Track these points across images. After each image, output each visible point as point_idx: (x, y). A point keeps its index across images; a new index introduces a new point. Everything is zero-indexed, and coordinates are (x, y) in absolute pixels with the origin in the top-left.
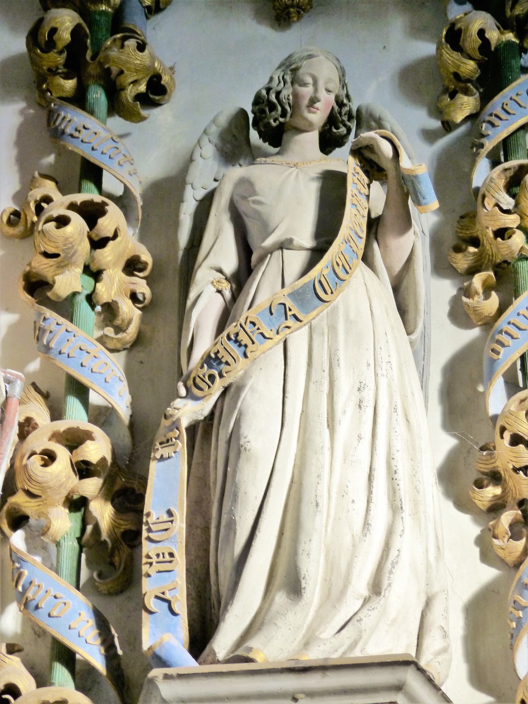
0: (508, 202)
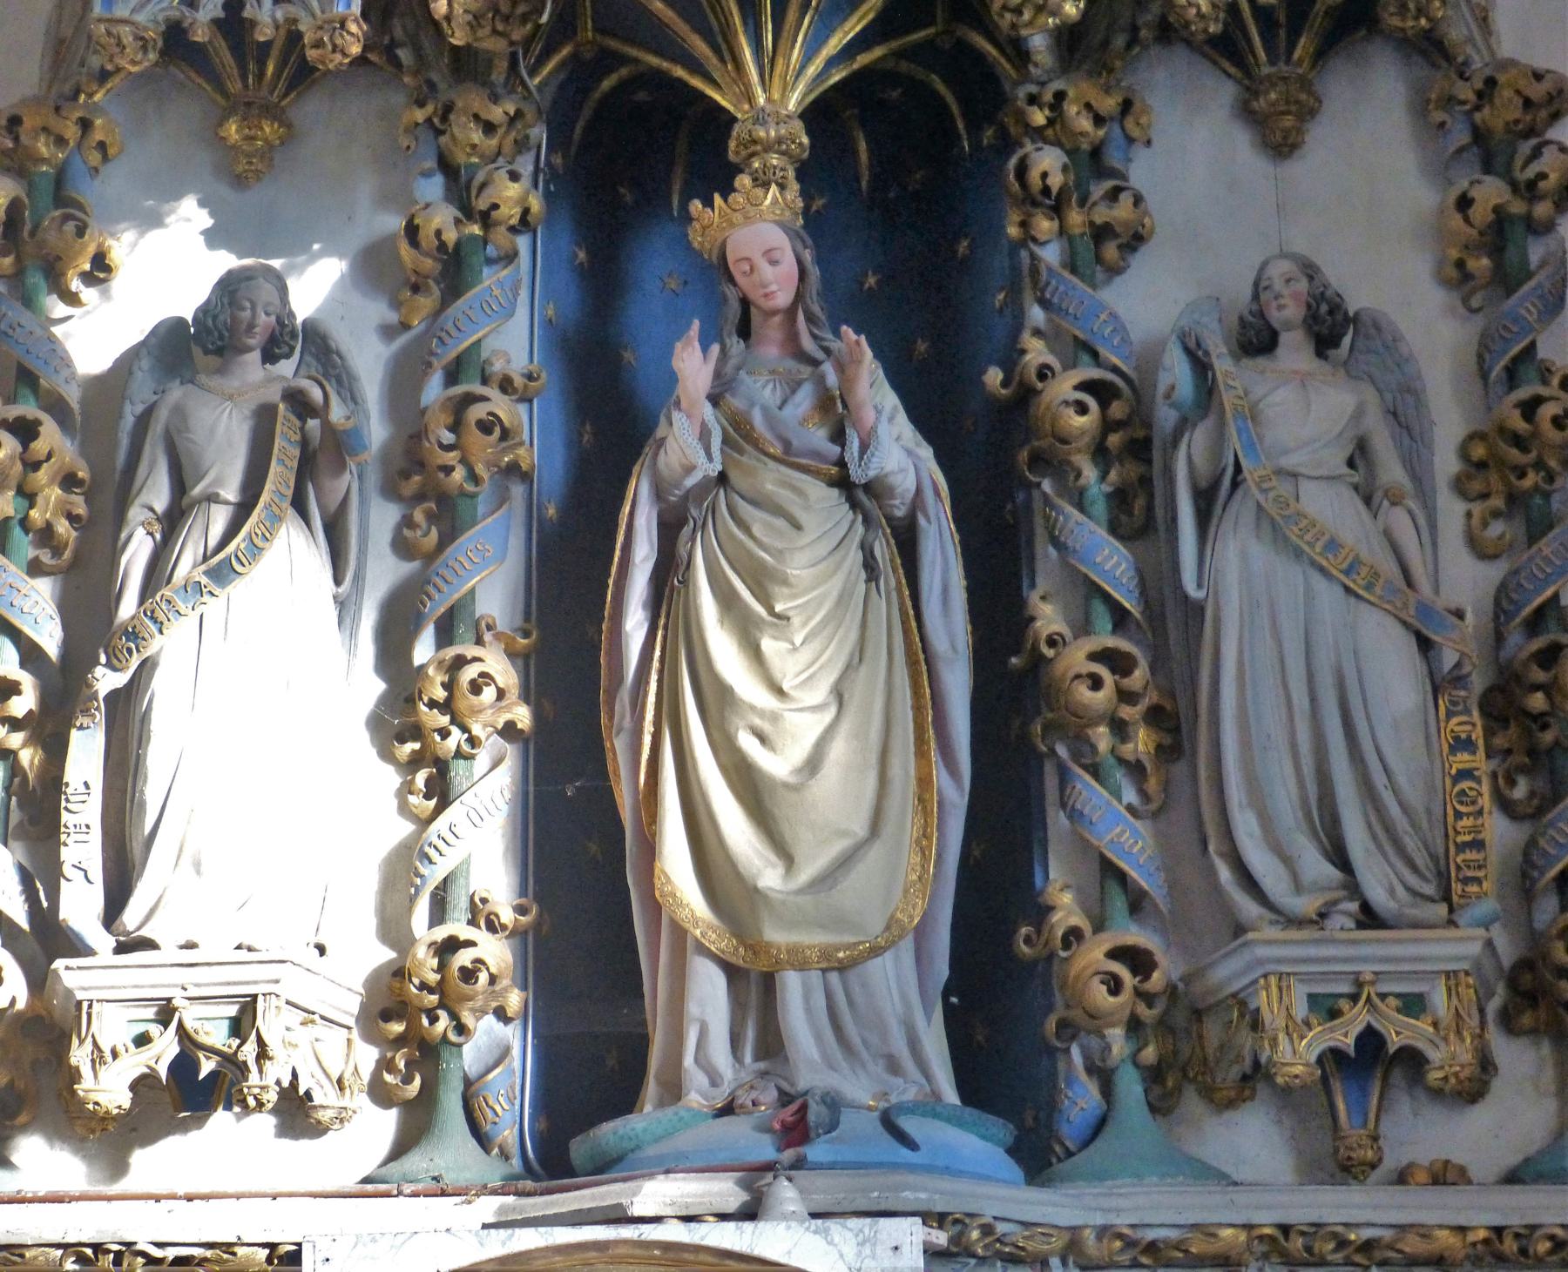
0: (448, 437)
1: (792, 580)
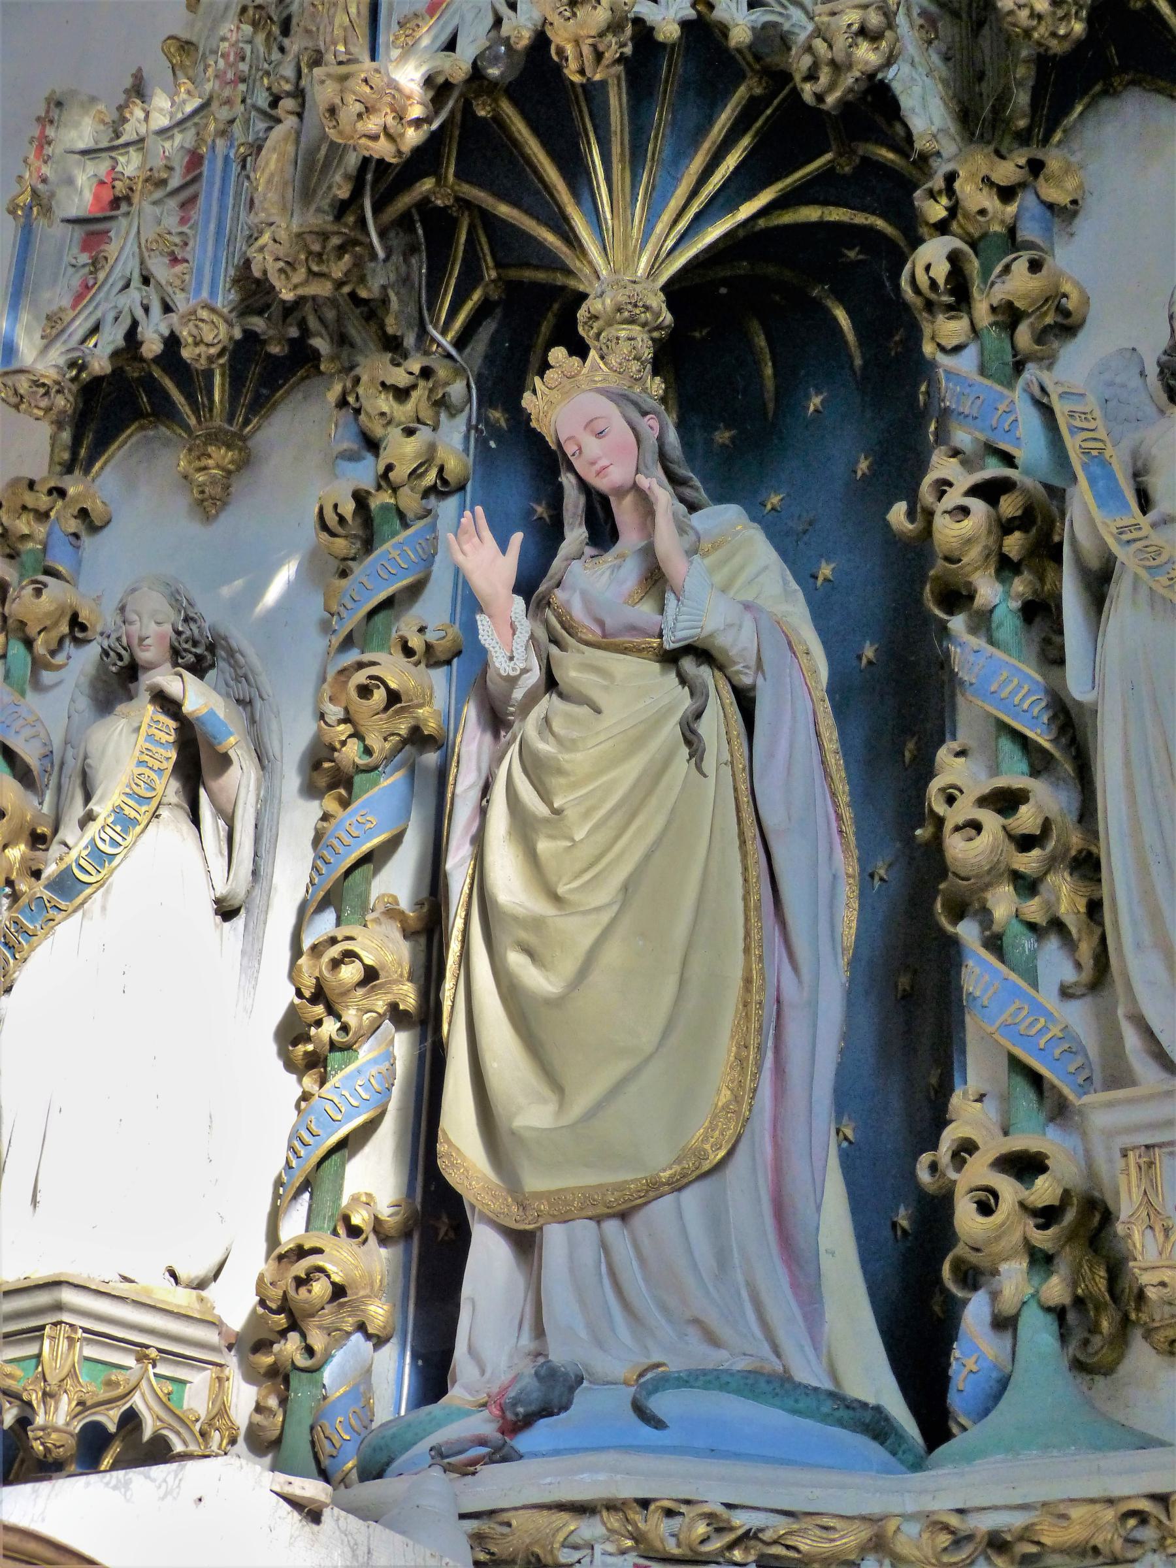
1: (567, 767)
